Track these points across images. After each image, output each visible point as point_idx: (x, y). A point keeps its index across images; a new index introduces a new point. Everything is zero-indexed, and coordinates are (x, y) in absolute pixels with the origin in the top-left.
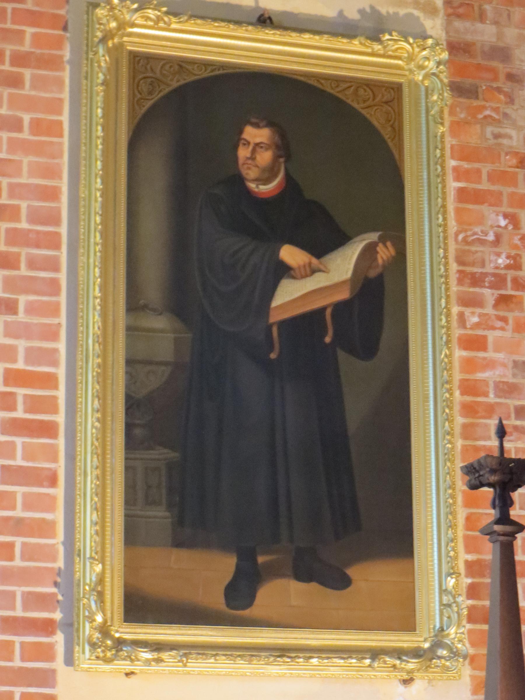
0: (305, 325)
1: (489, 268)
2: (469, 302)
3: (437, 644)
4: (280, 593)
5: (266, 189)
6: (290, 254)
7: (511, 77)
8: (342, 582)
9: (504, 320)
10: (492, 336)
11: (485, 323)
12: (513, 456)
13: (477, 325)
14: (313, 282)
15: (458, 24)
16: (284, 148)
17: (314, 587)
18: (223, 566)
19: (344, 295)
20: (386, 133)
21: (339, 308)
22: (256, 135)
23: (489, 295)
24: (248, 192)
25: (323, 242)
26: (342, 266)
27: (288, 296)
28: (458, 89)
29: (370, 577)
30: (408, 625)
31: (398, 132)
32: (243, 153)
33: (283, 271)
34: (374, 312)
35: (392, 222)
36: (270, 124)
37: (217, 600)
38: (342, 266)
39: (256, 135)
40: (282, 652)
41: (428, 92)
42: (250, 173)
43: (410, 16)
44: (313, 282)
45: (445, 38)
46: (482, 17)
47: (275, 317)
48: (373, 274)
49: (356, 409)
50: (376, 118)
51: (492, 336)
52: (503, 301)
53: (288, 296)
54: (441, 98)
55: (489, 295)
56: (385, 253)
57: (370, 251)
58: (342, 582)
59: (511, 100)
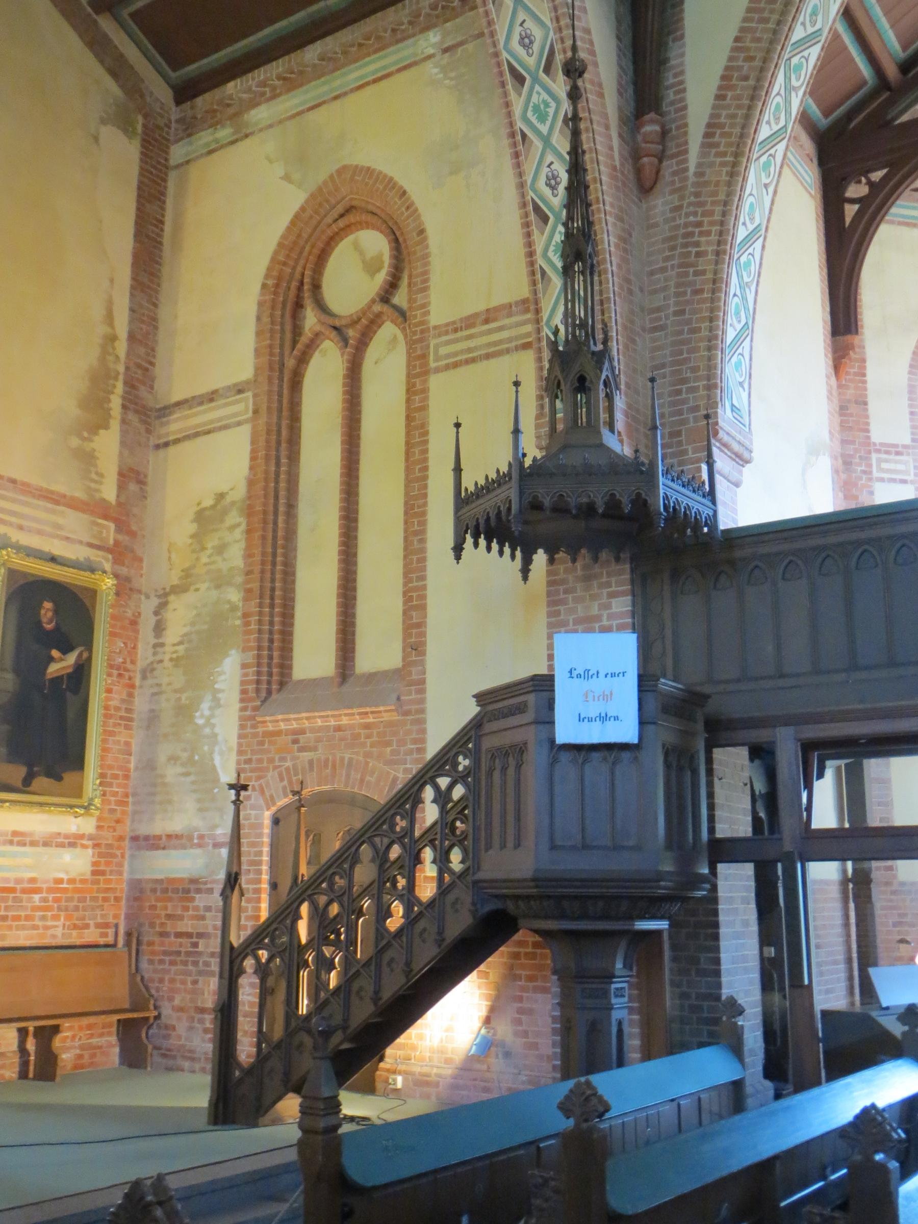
0: (57, 680)
1: (116, 663)
2: (109, 675)
3: (90, 804)
4: (41, 782)
5: (49, 627)
6: (55, 653)
7: (131, 589)
8: (59, 778)
9: (119, 682)
10: (115, 688)
11: (113, 684)
12: (417, 815)
13: (110, 684)
14: (61, 665)
15: (116, 567)
16: (56, 612)
17: (52, 780)
18: (22, 771)
19: (70, 670)
20: (90, 609)
21: (68, 674)
22: (48, 605)
23: (115, 672)
24: (42, 627)
25: (66, 649)
26: (71, 659)
27: (54, 669)
28: (117, 594)
29: (69, 777)
30: (79, 796)
31: (94, 607)
32: (43, 612)
33: (51, 659)
34: (80, 677)
35: (88, 644)
36: (53, 601)
37: (19, 784)
38: (71, 659)
39: (48, 605)
40: (41, 804)
41: (107, 595)
42: (44, 620)
43: (100, 562)
44: (61, 665)
45: (881, 1104)
46: (123, 565)
47: (48, 677)
48: (81, 662)
49: (71, 714)
50: (87, 602)
51: (115, 688)
52: (120, 675)
53: (54, 669)
54: (112, 597)
55: (115, 672)
56: (85, 655)
57: (80, 655)
58: (59, 778)
59: (130, 598)
